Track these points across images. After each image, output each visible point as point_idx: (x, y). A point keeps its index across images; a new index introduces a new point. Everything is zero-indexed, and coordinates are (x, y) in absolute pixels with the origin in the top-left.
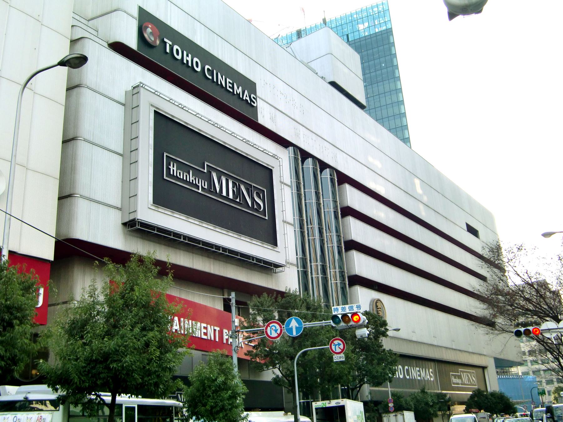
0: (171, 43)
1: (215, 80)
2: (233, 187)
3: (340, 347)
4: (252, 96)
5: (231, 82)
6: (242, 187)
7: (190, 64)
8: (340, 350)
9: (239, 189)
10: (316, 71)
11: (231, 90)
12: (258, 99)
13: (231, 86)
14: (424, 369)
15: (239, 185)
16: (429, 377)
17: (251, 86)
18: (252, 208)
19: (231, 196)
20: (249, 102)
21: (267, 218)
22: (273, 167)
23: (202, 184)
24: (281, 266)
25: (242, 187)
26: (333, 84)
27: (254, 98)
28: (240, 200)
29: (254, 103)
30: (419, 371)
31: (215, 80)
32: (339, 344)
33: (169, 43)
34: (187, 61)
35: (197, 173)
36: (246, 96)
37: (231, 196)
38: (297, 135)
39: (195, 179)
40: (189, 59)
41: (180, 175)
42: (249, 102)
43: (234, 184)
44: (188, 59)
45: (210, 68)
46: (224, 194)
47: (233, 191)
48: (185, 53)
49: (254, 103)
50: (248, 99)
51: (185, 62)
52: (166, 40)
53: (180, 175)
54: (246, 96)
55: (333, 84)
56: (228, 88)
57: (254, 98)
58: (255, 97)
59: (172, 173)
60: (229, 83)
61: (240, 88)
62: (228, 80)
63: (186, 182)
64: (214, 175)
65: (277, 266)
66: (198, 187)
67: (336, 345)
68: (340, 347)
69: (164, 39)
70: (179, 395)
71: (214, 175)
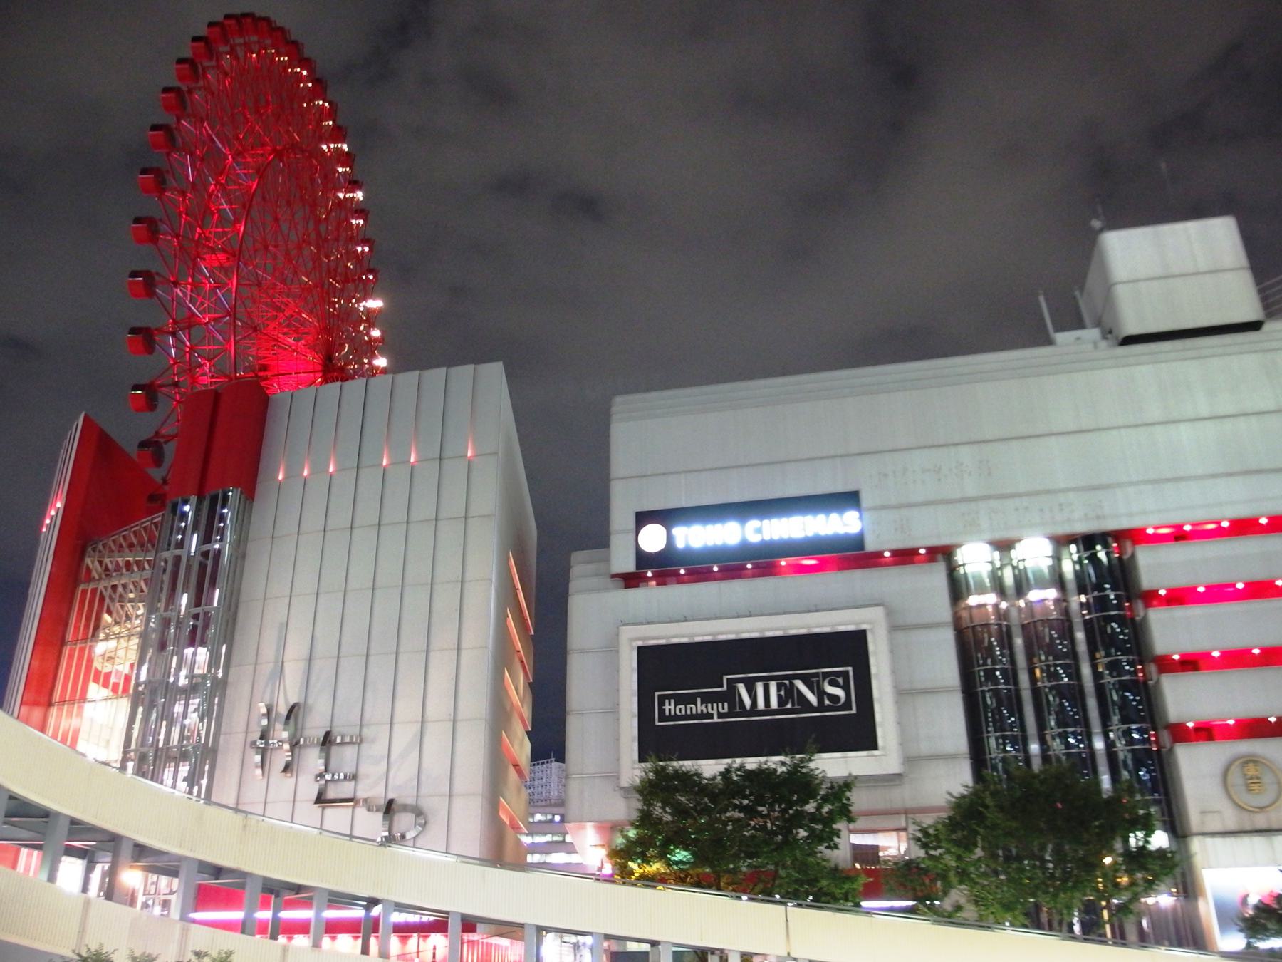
25: (800, 685)
39: (706, 707)
59: (667, 713)
66: (711, 716)
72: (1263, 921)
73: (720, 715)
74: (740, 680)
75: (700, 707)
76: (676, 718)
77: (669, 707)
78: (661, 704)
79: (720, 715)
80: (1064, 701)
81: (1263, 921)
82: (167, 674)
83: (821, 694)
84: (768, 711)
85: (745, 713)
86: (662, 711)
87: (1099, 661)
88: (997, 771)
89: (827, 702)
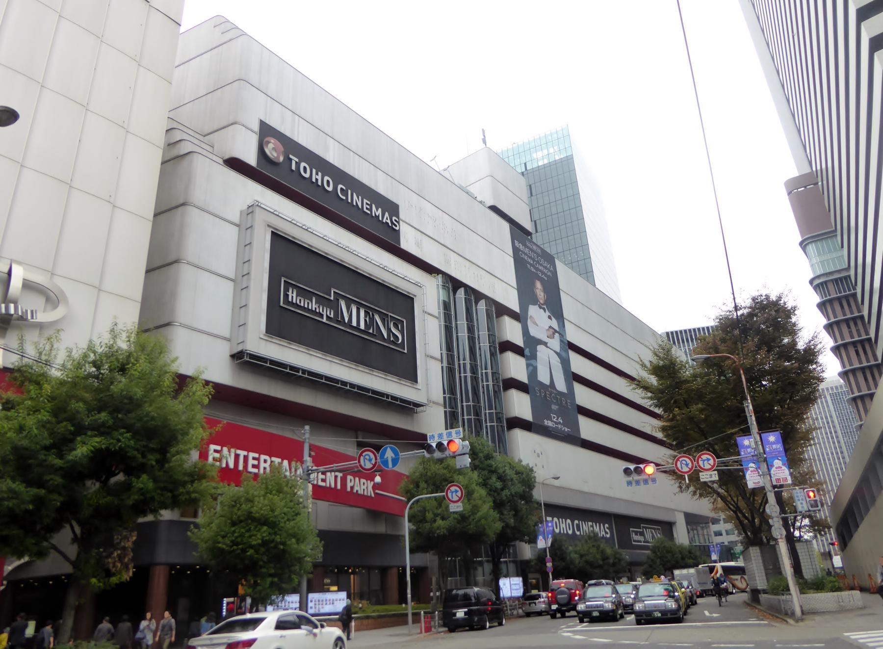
0: (297, 160)
1: (350, 201)
2: (366, 316)
3: (457, 494)
4: (394, 218)
5: (369, 203)
6: (377, 317)
7: (320, 183)
8: (457, 499)
9: (372, 319)
10: (474, 195)
11: (369, 212)
12: (401, 222)
13: (368, 207)
14: (598, 524)
15: (373, 314)
16: (604, 533)
17: (393, 208)
19: (362, 326)
20: (390, 225)
21: (406, 351)
22: (415, 296)
23: (327, 313)
24: (423, 406)
25: (377, 317)
26: (494, 209)
27: (395, 220)
28: (373, 331)
29: (396, 226)
30: (592, 526)
31: (350, 201)
32: (456, 491)
33: (295, 159)
34: (317, 180)
36: (387, 219)
37: (362, 326)
38: (447, 262)
39: (319, 307)
40: (319, 177)
41: (300, 302)
42: (390, 225)
43: (366, 313)
44: (317, 177)
45: (344, 188)
46: (354, 323)
47: (365, 320)
48: (314, 171)
49: (396, 226)
50: (389, 221)
51: (314, 180)
52: (291, 156)
53: (300, 302)
54: (387, 219)
55: (494, 209)
56: (365, 210)
57: (395, 220)
58: (397, 220)
59: (290, 299)
60: (367, 204)
61: (320, 174)
62: (365, 201)
63: (303, 308)
64: (343, 304)
65: (418, 405)
66: (321, 316)
67: (452, 492)
68: (457, 494)
69: (289, 156)
71: (343, 304)
72: (461, 592)
73: (328, 318)
74: (344, 297)
75: (313, 305)
76: (297, 306)
77: (293, 295)
78: (286, 290)
79: (328, 318)
80: (352, 568)
81: (461, 592)
82: (764, 501)
83: (389, 331)
84: (357, 328)
85: (342, 322)
86: (286, 296)
87: (856, 583)
88: (235, 530)
89: (392, 339)
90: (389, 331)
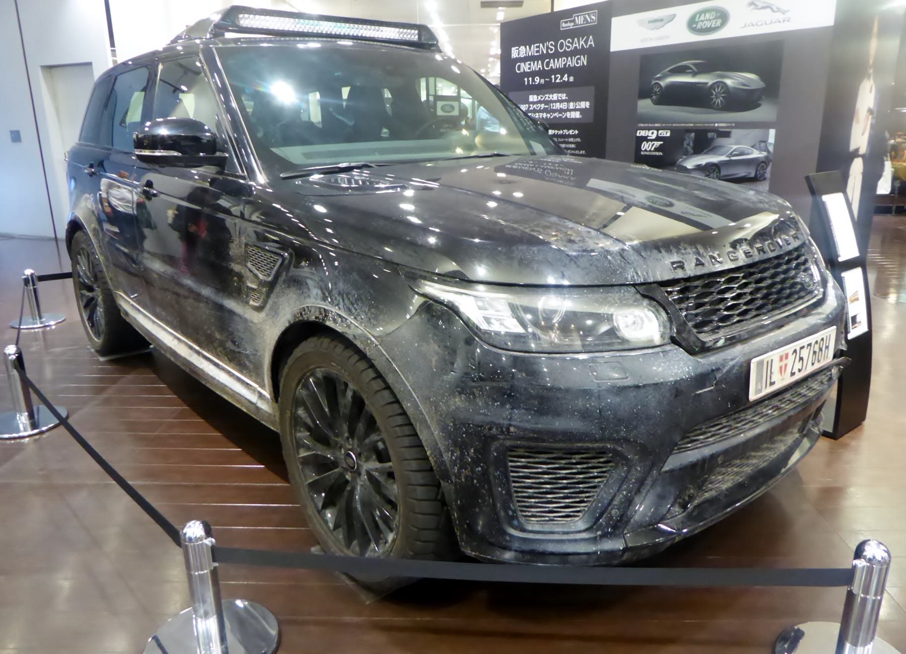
18: (591, 22)
30: (530, 64)
35: (571, 22)
70: (576, 18)
83: (591, 19)
90: (591, 19)
